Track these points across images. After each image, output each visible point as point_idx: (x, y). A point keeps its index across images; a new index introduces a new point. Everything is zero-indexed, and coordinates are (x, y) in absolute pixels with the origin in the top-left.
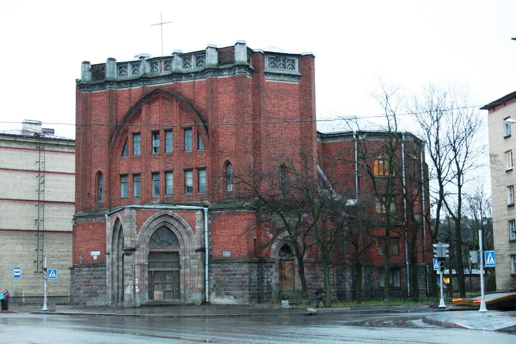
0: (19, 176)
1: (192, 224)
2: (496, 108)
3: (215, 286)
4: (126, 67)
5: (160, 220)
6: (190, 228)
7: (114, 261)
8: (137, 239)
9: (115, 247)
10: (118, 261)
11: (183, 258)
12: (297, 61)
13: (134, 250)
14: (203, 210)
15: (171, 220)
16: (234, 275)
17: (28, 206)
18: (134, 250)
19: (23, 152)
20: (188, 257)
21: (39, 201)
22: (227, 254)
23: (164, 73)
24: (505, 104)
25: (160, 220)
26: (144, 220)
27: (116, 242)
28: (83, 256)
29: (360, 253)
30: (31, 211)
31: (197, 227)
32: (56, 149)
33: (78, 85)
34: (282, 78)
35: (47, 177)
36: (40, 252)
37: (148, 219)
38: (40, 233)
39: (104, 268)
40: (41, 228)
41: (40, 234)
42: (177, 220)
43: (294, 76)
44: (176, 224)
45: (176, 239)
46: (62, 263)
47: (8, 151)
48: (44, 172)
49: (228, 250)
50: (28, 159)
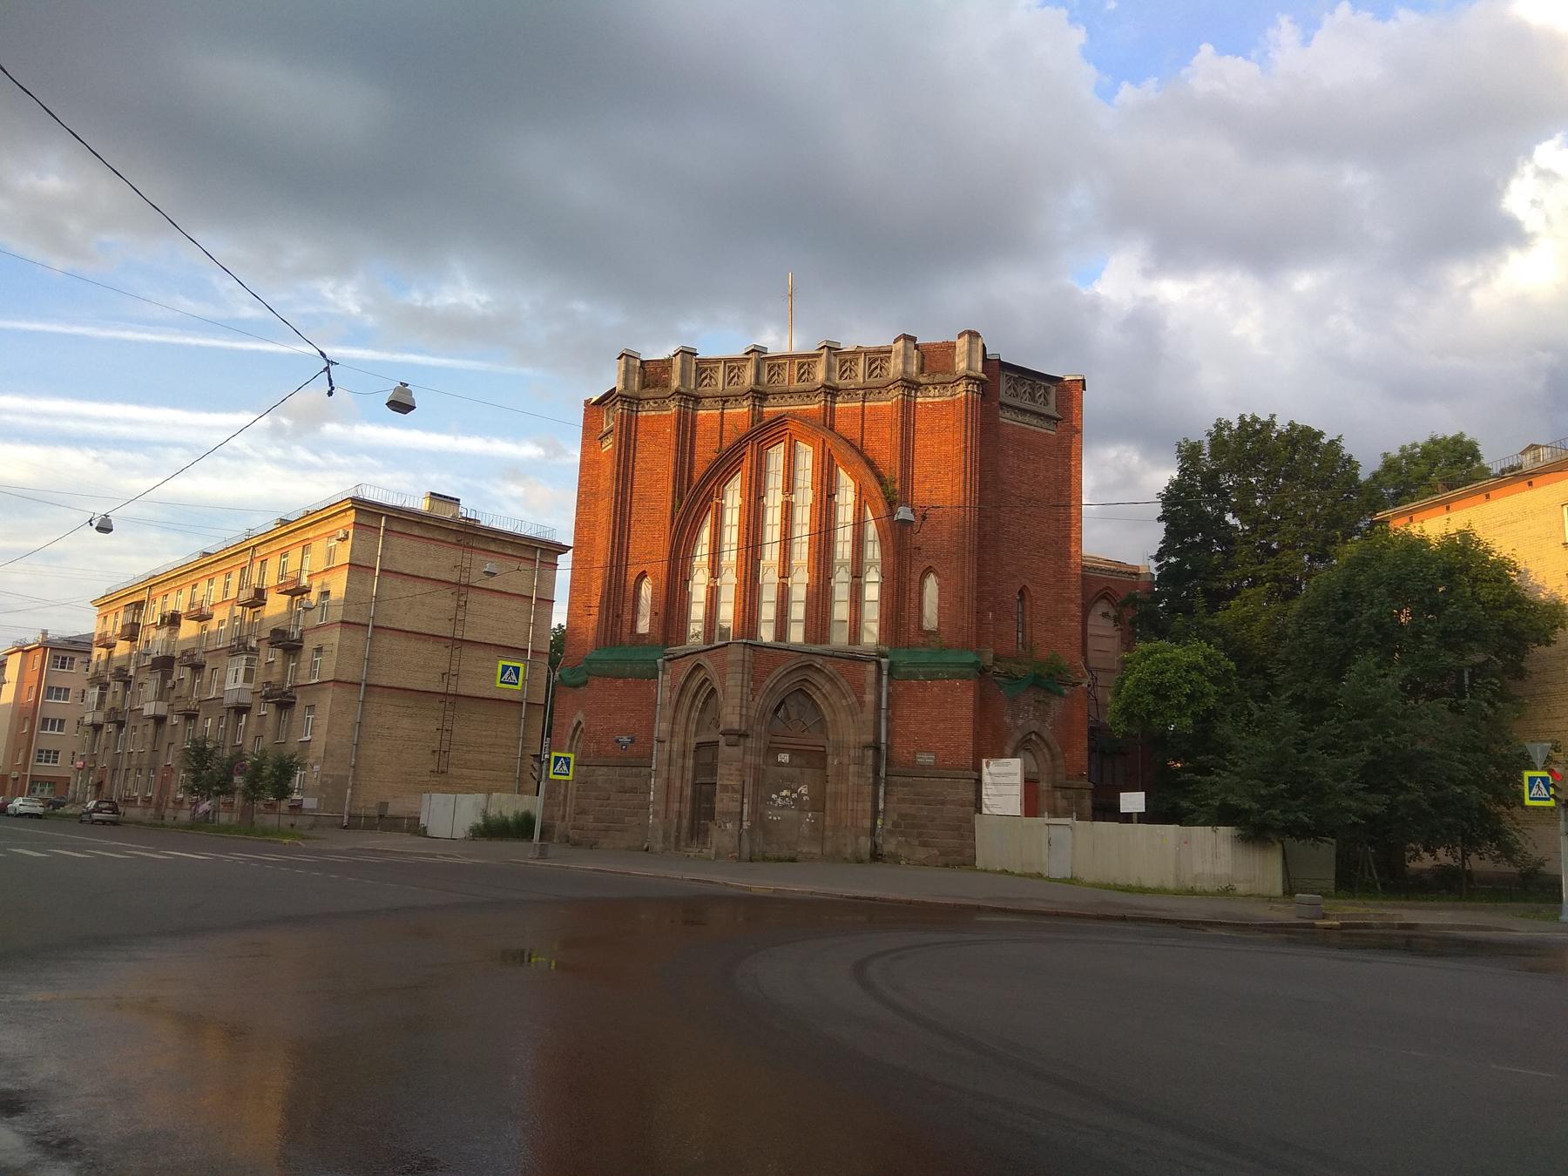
0: (420, 588)
1: (859, 690)
2: (1452, 506)
3: (896, 825)
4: (715, 370)
5: (796, 678)
6: (854, 698)
7: (674, 756)
8: (752, 713)
9: (679, 728)
10: (684, 757)
11: (833, 761)
12: (1053, 390)
13: (744, 735)
14: (879, 663)
15: (816, 676)
16: (943, 803)
17: (427, 647)
18: (744, 735)
19: (415, 544)
20: (846, 761)
21: (453, 639)
22: (926, 759)
23: (796, 385)
24: (1530, 484)
25: (796, 678)
26: (769, 673)
27: (682, 717)
28: (598, 743)
29: (1238, 774)
30: (439, 657)
31: (869, 697)
32: (493, 547)
33: (281, 626)
34: (1027, 419)
35: (472, 596)
36: (446, 736)
37: (776, 672)
38: (453, 700)
39: (644, 771)
40: (452, 690)
41: (450, 699)
42: (831, 679)
43: (1049, 418)
44: (827, 687)
45: (822, 721)
46: (484, 757)
47: (404, 541)
48: (467, 586)
49: (929, 751)
50: (440, 561)
